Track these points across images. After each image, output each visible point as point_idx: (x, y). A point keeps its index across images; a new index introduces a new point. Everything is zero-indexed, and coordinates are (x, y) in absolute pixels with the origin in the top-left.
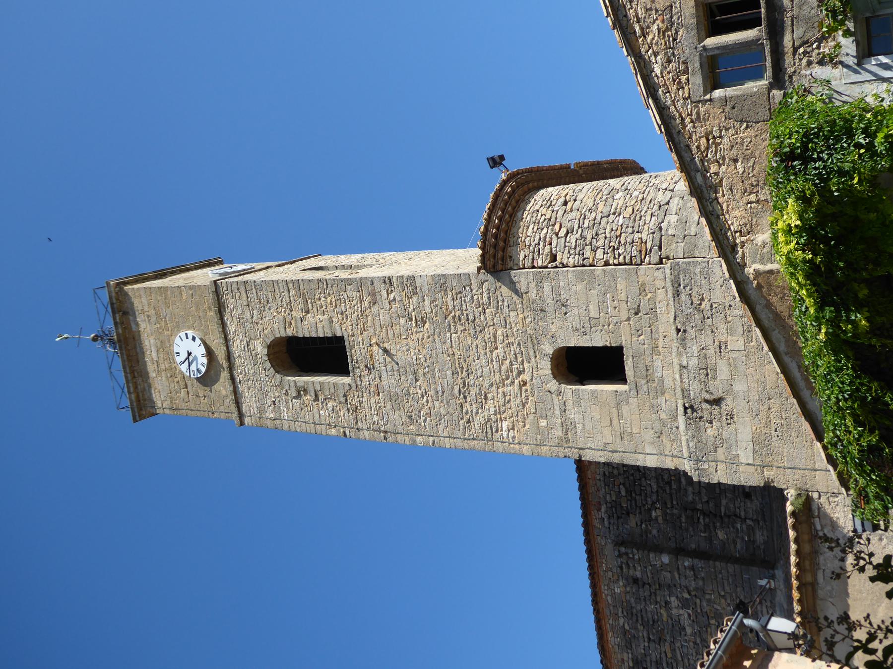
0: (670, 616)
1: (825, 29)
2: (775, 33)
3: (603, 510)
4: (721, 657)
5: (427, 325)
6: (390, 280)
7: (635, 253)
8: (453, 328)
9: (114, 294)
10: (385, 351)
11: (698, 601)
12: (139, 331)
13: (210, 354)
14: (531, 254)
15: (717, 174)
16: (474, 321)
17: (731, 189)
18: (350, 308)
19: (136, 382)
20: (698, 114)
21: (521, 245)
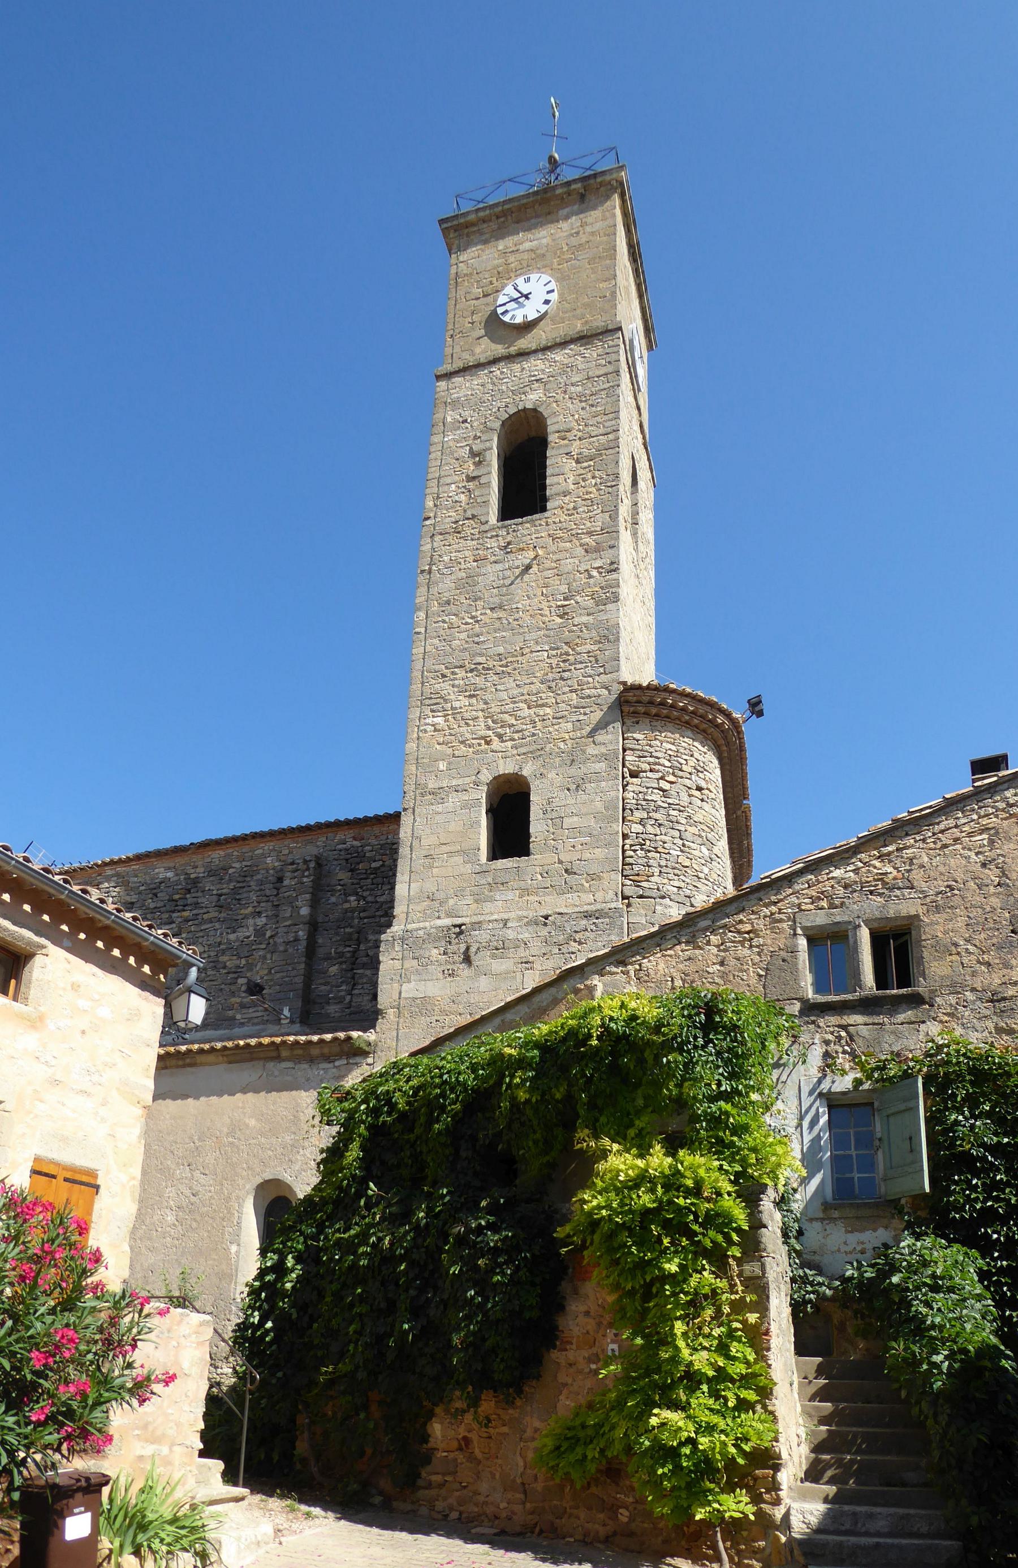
0: (246, 917)
1: (863, 1058)
2: (867, 1006)
3: (356, 843)
4: (147, 940)
5: (559, 620)
6: (615, 570)
7: (636, 868)
8: (554, 652)
9: (607, 178)
10: (528, 567)
11: (263, 946)
12: (558, 221)
13: (528, 326)
14: (640, 747)
15: (708, 943)
16: (562, 679)
17: (690, 959)
18: (582, 519)
19: (490, 220)
20: (781, 921)
21: (652, 735)
